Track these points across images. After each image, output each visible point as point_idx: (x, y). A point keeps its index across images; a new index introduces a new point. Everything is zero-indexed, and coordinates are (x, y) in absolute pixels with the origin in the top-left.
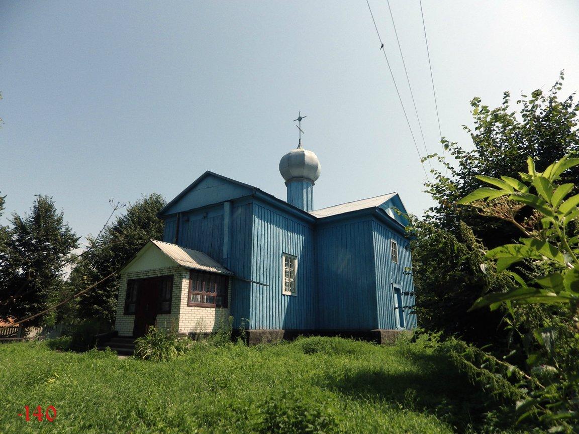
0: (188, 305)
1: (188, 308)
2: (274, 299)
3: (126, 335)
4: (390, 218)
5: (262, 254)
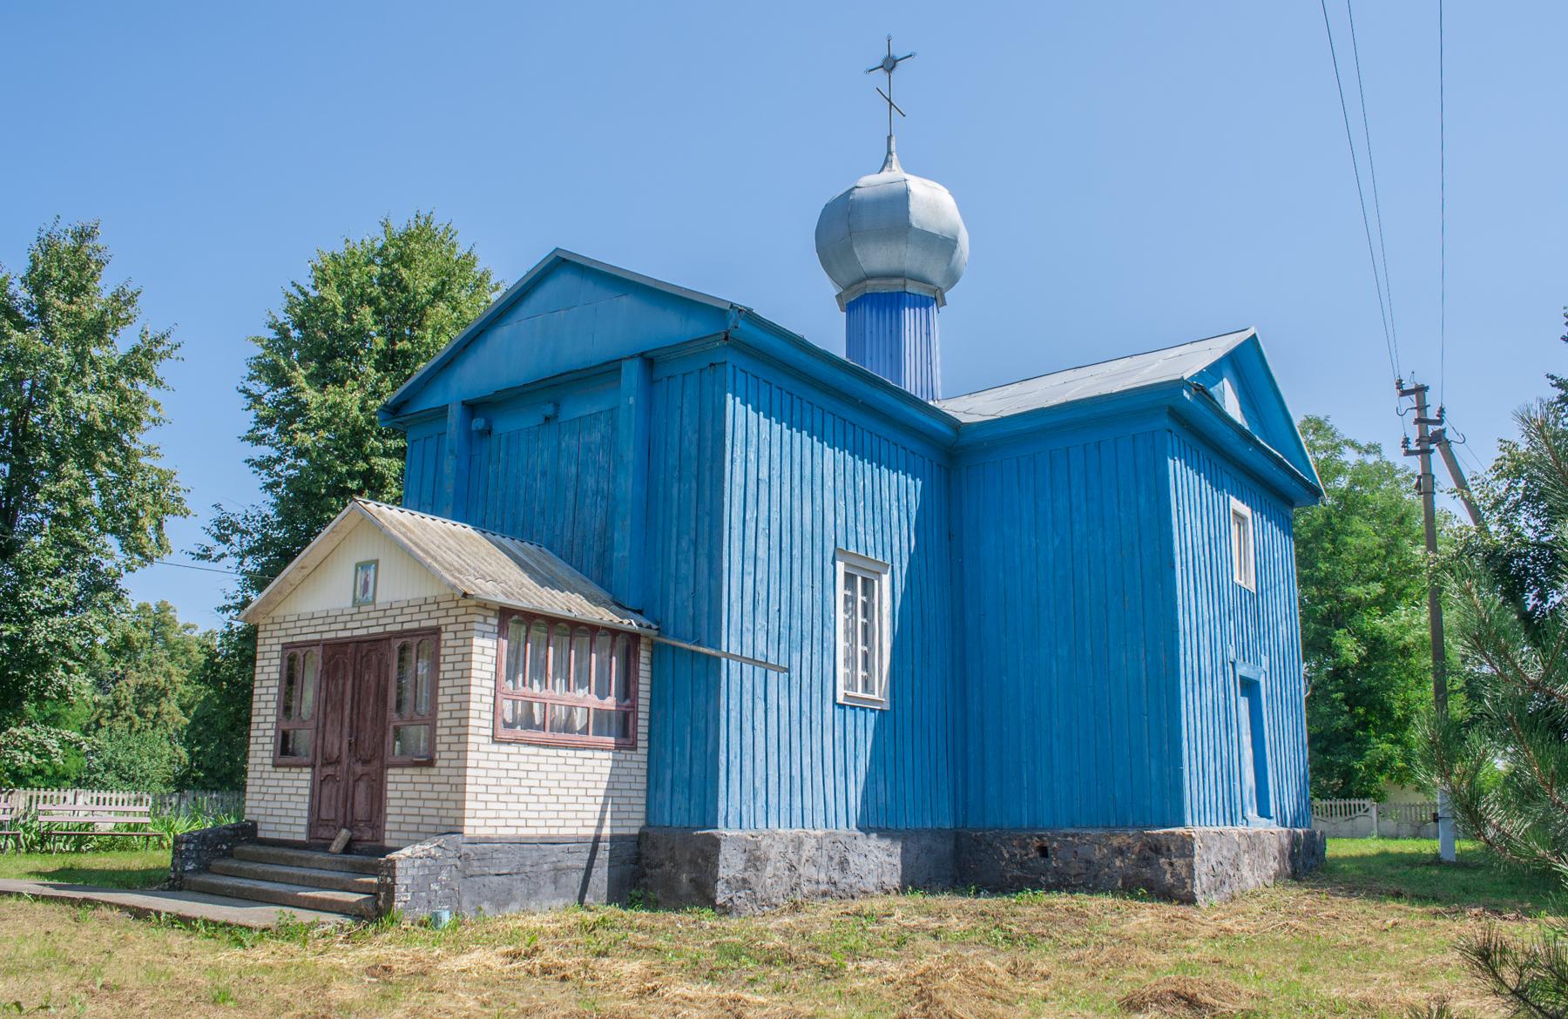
0: (496, 740)
1: (495, 748)
2: (805, 721)
3: (284, 836)
4: (1230, 422)
5: (762, 553)
